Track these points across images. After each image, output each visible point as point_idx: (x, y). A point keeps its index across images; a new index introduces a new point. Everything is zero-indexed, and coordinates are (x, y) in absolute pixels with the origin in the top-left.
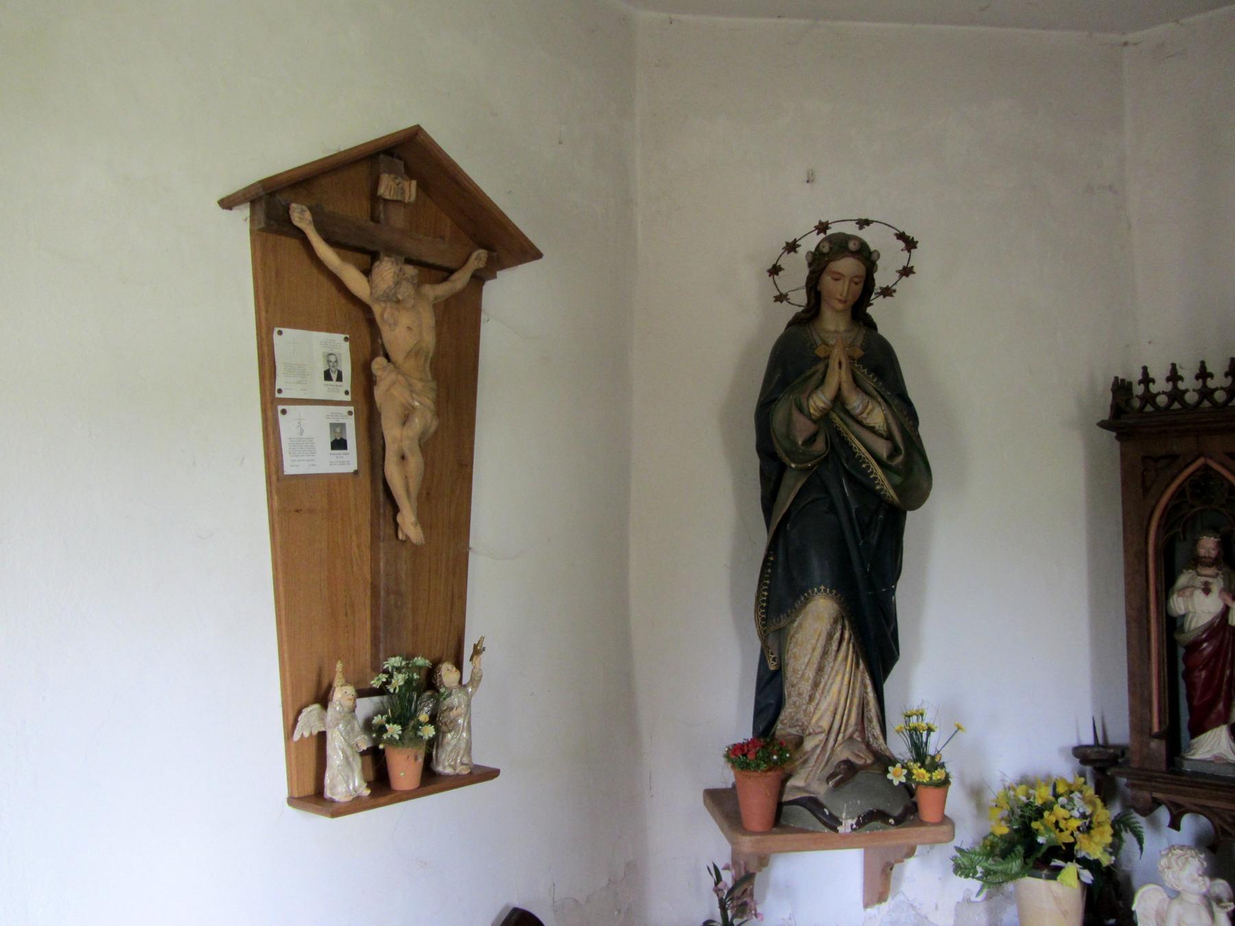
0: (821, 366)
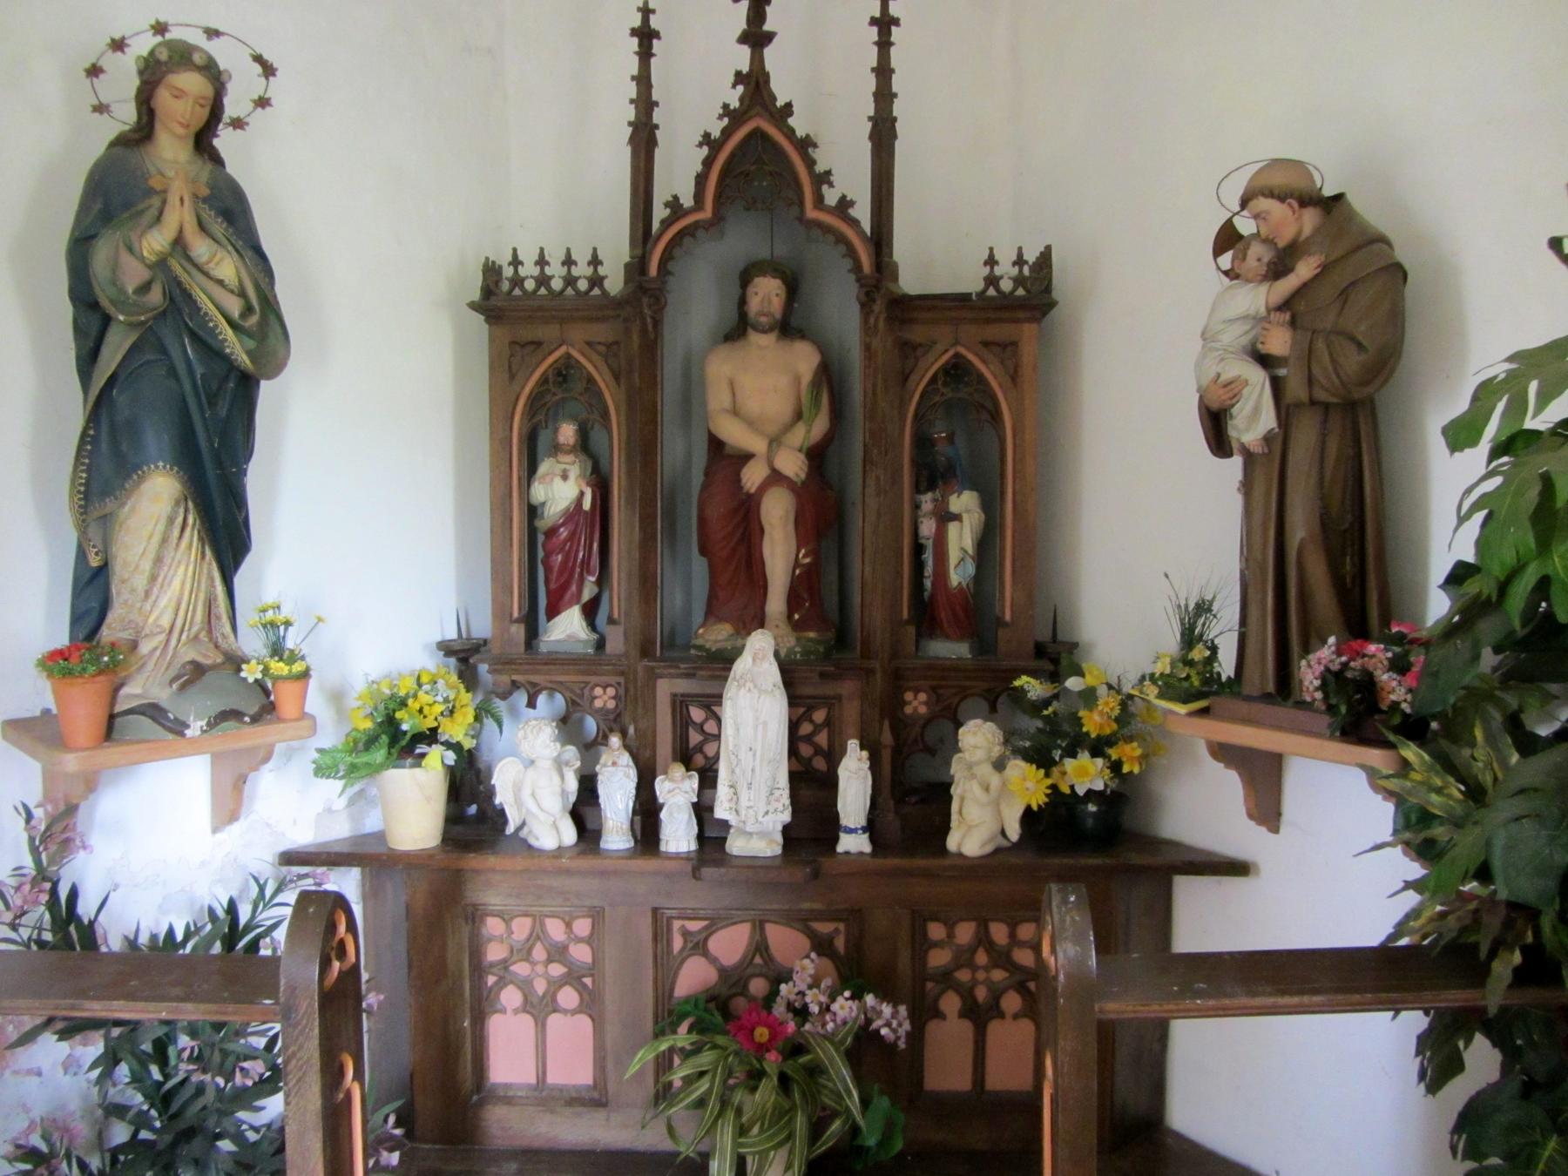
0: (155, 202)
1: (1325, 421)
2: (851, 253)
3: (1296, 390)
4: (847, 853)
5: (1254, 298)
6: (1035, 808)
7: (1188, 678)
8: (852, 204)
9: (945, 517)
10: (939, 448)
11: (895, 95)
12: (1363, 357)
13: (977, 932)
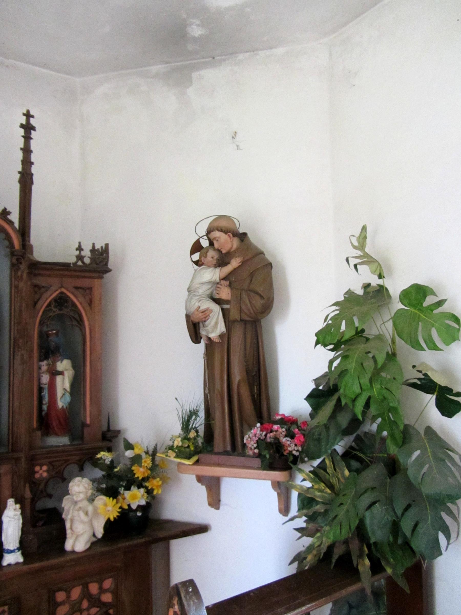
1: (245, 328)
2: (8, 238)
3: (234, 315)
4: (9, 565)
5: (211, 275)
6: (112, 519)
7: (188, 447)
8: (9, 213)
9: (54, 373)
10: (52, 338)
11: (32, 163)
12: (262, 302)
13: (83, 591)
